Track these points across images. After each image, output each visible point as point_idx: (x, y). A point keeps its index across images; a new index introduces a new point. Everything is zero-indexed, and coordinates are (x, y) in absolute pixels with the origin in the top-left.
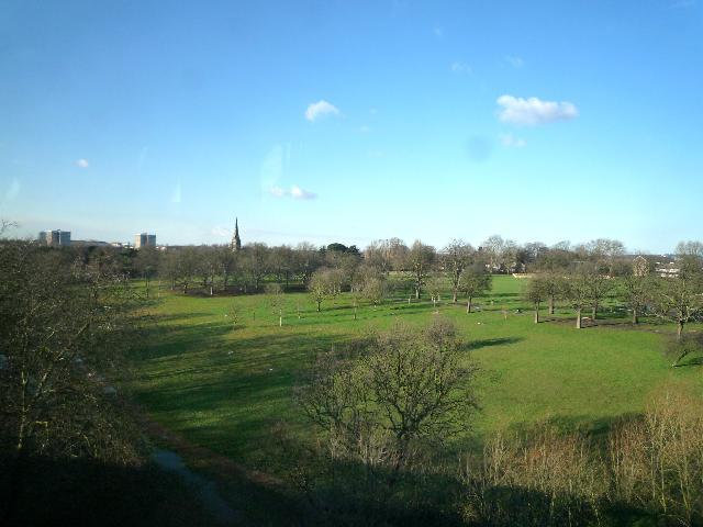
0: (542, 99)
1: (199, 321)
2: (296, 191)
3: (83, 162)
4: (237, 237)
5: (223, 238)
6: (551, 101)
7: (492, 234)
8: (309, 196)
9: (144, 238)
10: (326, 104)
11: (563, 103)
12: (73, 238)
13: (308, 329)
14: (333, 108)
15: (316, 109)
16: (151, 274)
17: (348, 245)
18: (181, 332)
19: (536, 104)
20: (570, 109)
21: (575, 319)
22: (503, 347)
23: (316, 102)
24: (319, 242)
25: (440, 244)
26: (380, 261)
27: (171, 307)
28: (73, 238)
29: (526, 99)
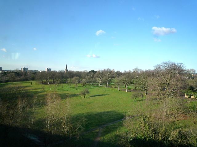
0: (166, 27)
1: (37, 90)
2: (94, 56)
3: (35, 49)
4: (67, 70)
5: (64, 69)
6: (168, 28)
7: (135, 67)
8: (97, 57)
9: (48, 69)
10: (102, 31)
11: (172, 28)
12: (52, 70)
13: (62, 92)
14: (104, 32)
15: (99, 32)
16: (33, 79)
17: (95, 70)
18: (30, 93)
19: (164, 29)
20: (174, 30)
21: (126, 90)
22: (103, 96)
23: (99, 30)
24: (89, 70)
25: (122, 71)
26: (102, 74)
27: (33, 86)
28: (52, 70)
29: (161, 27)
